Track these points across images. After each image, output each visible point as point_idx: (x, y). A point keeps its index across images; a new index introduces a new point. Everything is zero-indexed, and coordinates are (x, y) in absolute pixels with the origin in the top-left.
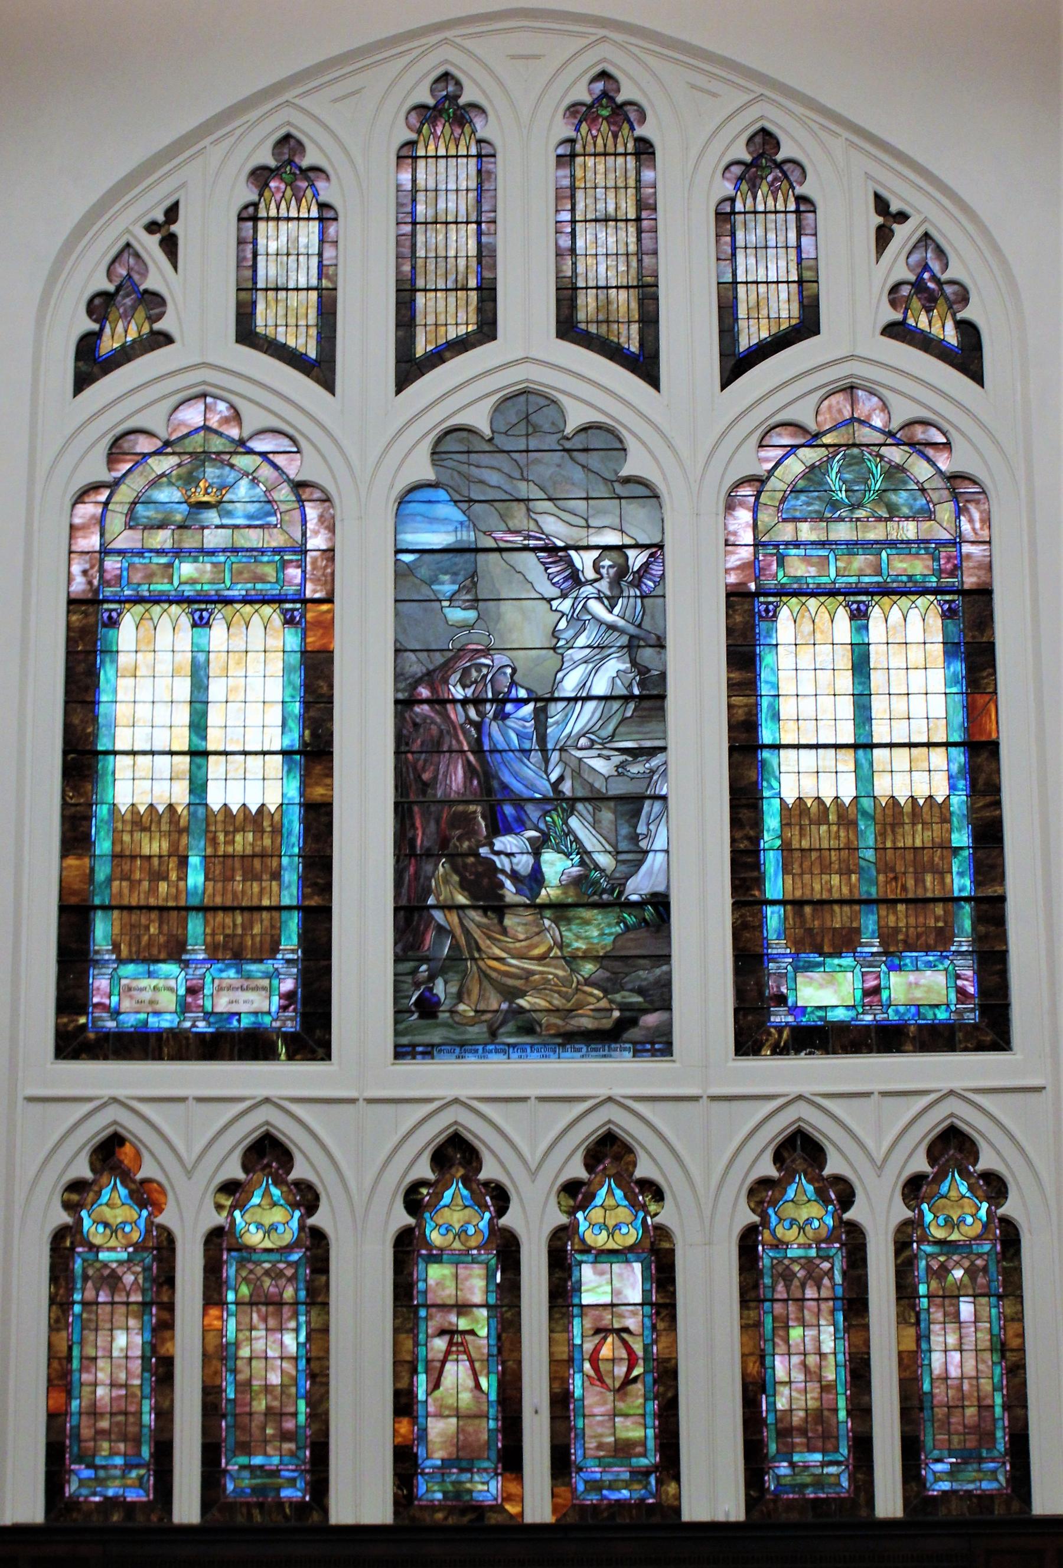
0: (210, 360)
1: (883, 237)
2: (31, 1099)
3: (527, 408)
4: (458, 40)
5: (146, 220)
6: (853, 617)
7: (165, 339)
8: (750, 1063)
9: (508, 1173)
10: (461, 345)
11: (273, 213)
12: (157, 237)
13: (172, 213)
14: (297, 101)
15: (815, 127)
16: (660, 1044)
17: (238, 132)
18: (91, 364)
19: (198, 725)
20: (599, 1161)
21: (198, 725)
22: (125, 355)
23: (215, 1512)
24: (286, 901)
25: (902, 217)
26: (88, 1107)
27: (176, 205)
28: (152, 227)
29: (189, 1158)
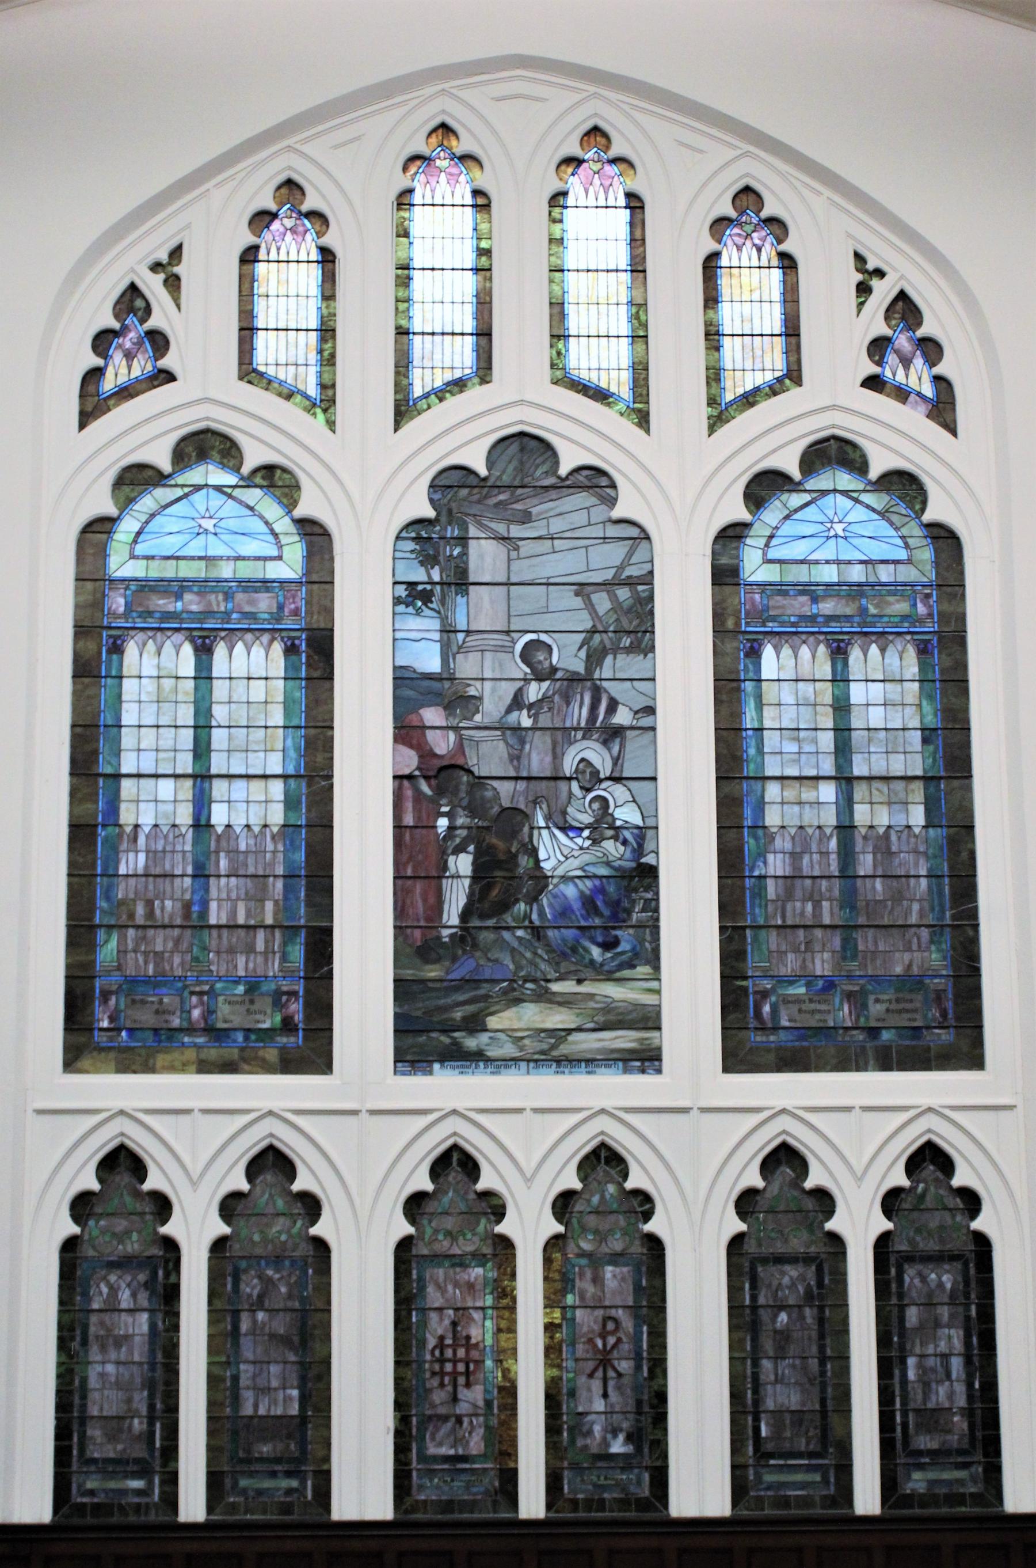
0: (528, 397)
1: (863, 289)
2: (40, 1112)
3: (525, 450)
4: (452, 91)
5: (151, 260)
6: (197, 650)
7: (167, 377)
8: (418, 1081)
9: (980, 1178)
10: (775, 389)
11: (273, 256)
12: (162, 276)
13: (176, 253)
14: (297, 146)
15: (798, 184)
16: (648, 1059)
17: (239, 177)
18: (93, 402)
19: (201, 750)
20: (259, 1172)
21: (201, 750)
22: (126, 393)
23: (65, 1510)
24: (914, 919)
25: (880, 273)
26: (905, 1116)
27: (180, 247)
28: (156, 267)
29: (529, 1168)
